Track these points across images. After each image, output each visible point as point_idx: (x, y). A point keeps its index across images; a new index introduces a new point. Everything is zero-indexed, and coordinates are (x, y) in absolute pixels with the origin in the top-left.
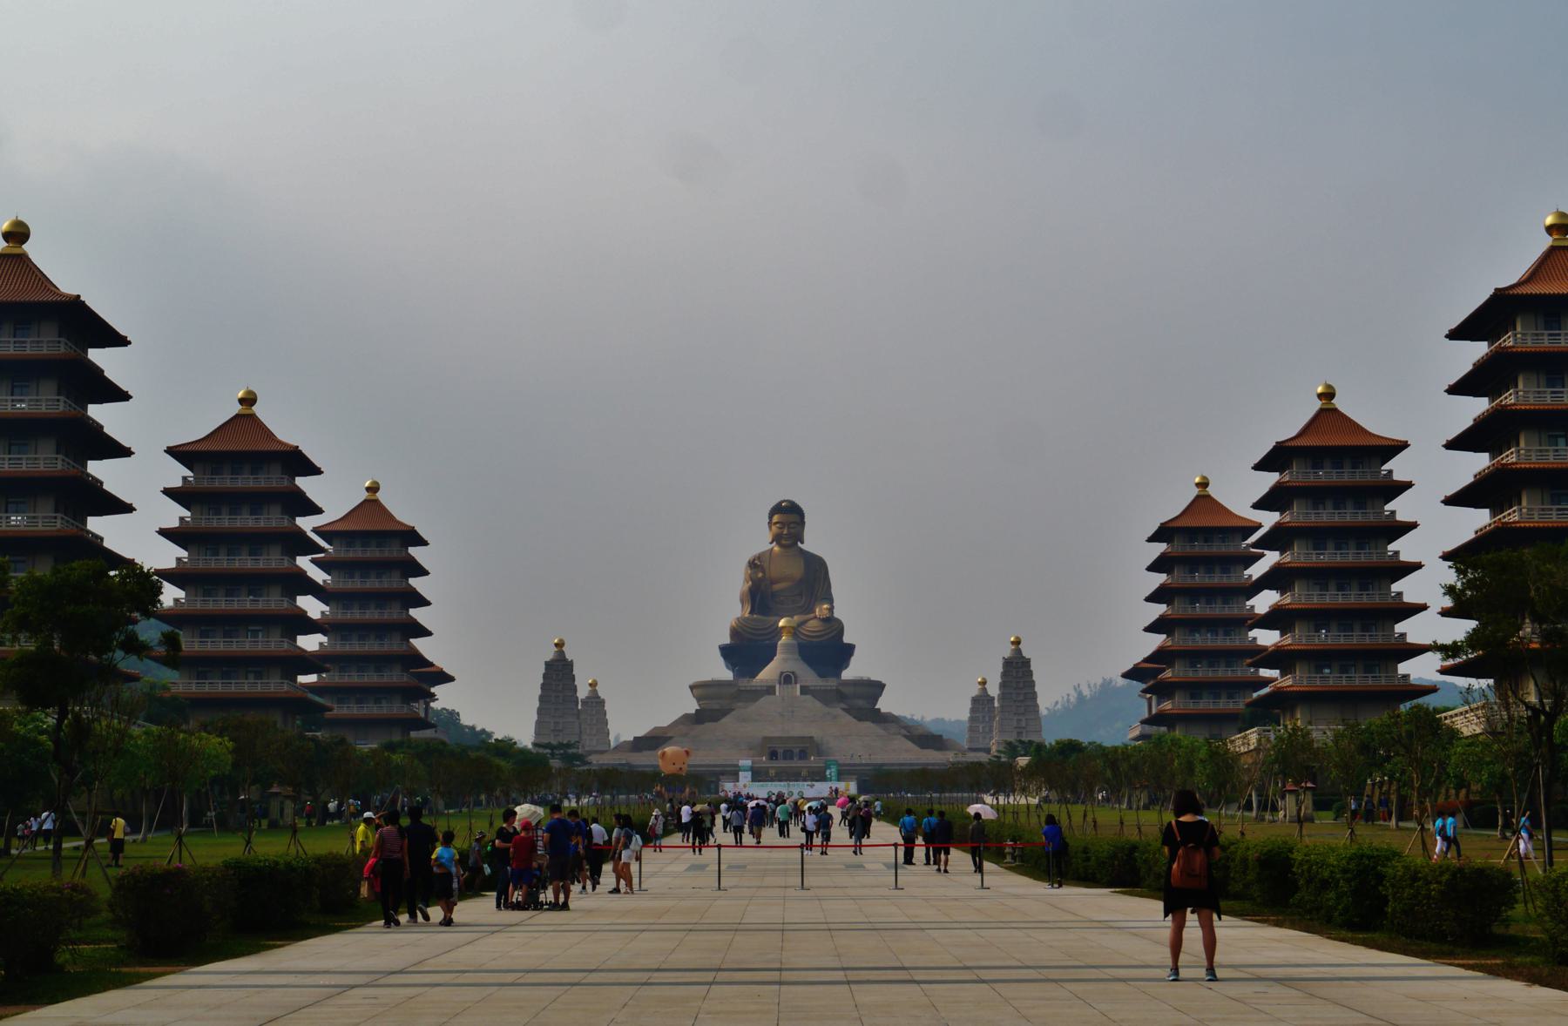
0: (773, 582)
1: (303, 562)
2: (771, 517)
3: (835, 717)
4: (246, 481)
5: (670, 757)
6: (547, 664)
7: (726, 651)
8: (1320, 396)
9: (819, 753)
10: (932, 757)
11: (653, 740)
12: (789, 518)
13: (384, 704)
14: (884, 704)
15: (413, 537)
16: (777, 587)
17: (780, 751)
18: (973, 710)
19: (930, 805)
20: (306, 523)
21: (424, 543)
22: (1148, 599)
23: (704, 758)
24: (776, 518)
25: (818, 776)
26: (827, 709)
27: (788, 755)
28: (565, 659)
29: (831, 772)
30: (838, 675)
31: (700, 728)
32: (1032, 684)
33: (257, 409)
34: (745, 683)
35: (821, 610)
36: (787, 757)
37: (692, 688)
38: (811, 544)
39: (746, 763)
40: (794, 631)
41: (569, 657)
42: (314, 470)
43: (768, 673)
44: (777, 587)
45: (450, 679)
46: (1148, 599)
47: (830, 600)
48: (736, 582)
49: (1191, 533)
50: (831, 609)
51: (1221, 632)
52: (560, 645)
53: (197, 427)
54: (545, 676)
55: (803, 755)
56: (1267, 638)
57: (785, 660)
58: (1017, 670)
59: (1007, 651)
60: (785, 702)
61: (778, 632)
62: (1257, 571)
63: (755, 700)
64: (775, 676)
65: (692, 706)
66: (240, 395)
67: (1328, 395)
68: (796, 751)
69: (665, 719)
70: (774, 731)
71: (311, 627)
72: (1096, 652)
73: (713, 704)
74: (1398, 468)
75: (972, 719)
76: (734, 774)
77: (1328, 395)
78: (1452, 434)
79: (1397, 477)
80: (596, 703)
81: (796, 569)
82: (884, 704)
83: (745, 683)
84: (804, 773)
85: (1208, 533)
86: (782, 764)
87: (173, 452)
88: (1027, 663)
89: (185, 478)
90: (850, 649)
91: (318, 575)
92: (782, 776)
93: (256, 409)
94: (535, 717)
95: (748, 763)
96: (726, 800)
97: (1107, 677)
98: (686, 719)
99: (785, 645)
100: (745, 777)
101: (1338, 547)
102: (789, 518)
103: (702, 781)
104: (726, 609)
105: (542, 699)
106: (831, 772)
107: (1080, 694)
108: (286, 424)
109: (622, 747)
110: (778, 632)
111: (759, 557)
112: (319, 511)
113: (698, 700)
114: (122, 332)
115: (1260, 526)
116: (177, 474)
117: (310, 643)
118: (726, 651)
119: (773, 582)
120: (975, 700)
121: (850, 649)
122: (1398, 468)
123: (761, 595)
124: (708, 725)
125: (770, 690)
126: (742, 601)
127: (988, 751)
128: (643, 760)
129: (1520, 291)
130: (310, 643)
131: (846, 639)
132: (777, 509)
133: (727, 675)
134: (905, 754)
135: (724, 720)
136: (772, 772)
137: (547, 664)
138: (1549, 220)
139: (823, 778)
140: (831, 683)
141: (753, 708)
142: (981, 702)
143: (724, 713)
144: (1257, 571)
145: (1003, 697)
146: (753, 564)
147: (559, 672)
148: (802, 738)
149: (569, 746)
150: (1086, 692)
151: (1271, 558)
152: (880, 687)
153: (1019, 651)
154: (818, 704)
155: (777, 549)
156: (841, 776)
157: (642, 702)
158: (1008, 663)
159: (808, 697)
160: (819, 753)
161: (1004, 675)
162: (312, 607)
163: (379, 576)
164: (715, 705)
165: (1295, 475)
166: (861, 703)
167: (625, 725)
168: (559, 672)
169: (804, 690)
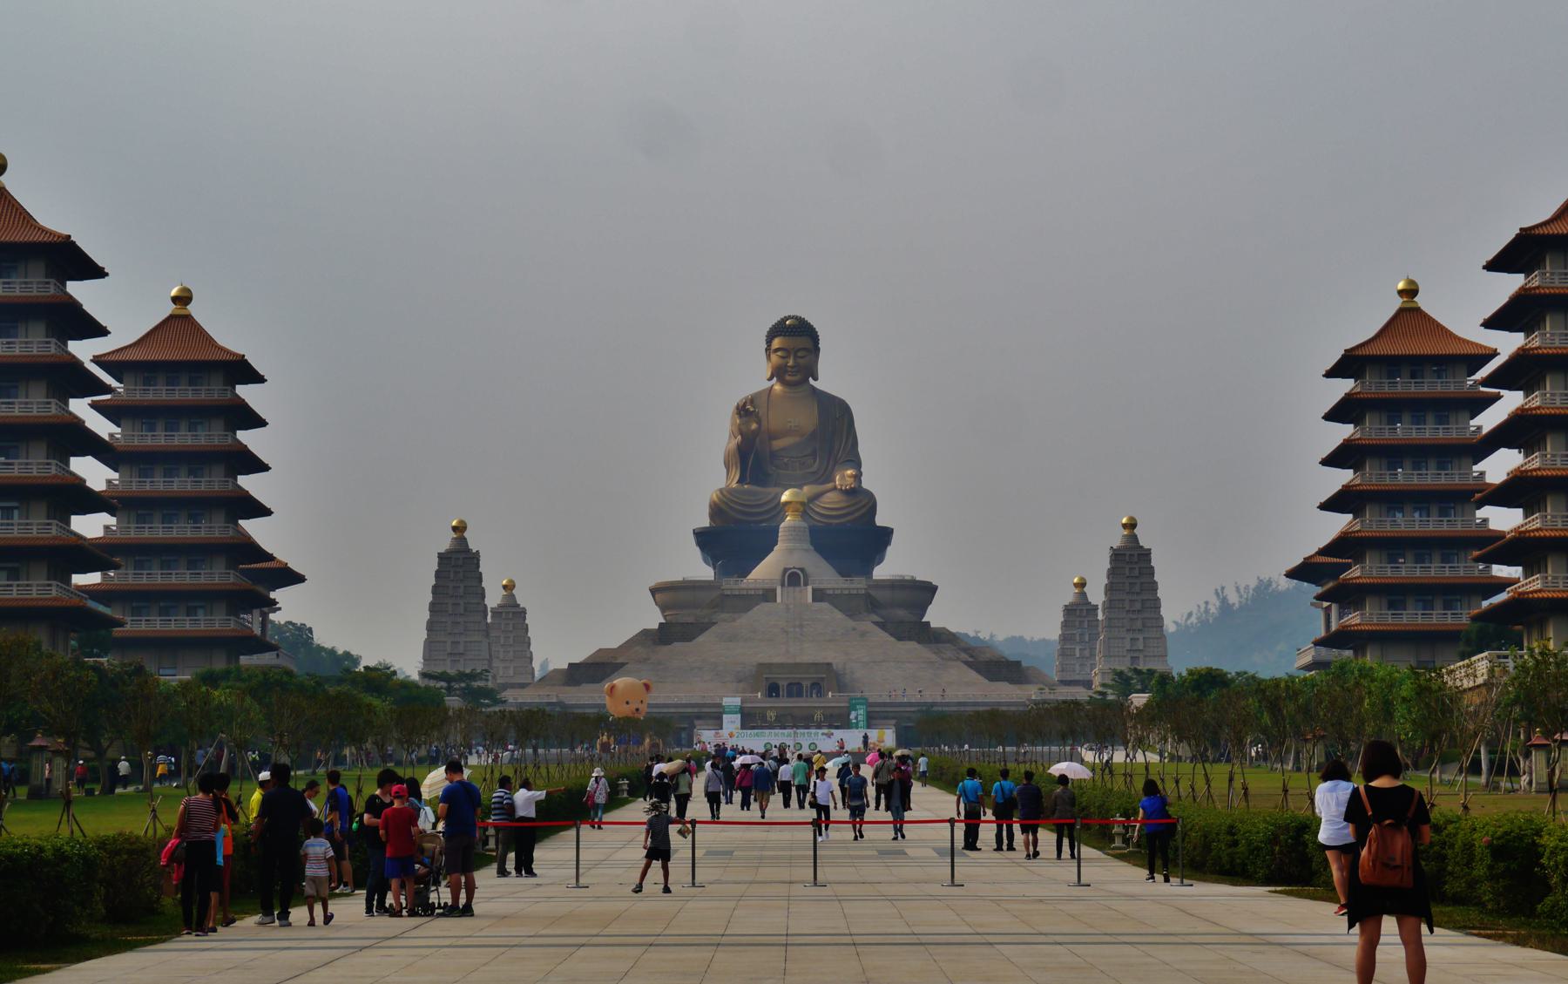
0: (773, 436)
1: (80, 407)
3: (863, 634)
5: (621, 694)
6: (441, 556)
7: (704, 539)
8: (1401, 293)
9: (841, 687)
10: (1005, 694)
11: (596, 669)
12: (796, 342)
13: (201, 615)
14: (935, 616)
15: (71, 260)
17: (783, 684)
18: (1065, 625)
20: (83, 350)
23: (672, 694)
24: (776, 343)
26: (851, 623)
27: (795, 690)
28: (469, 551)
29: (858, 714)
30: (869, 573)
32: (1153, 587)
33: (192, 309)
34: (731, 585)
35: (844, 477)
36: (791, 693)
37: (653, 591)
38: (828, 380)
40: (804, 509)
41: (473, 546)
42: (256, 378)
43: (766, 570)
47: (857, 464)
48: (721, 436)
50: (858, 477)
52: (460, 529)
54: (438, 574)
55: (817, 688)
56: (1504, 519)
57: (790, 551)
58: (1132, 566)
59: (1117, 538)
61: (779, 510)
62: (1489, 420)
63: (747, 609)
65: (653, 618)
66: (174, 292)
71: (90, 502)
72: (1248, 537)
73: (684, 615)
75: (1065, 638)
76: (715, 717)
77: (1410, 292)
80: (513, 613)
81: (805, 418)
82: (935, 616)
83: (731, 585)
84: (818, 716)
85: (1417, 364)
86: (785, 703)
88: (1146, 555)
90: (885, 535)
91: (102, 427)
92: (782, 721)
95: (737, 701)
98: (647, 638)
99: (793, 529)
100: (731, 722)
102: (796, 342)
104: (709, 476)
105: (433, 607)
106: (858, 714)
107: (1224, 601)
108: (227, 329)
109: (551, 678)
110: (779, 510)
111: (752, 400)
112: (101, 331)
115: (1494, 354)
117: (90, 526)
118: (704, 539)
119: (773, 436)
120: (1069, 610)
121: (885, 535)
123: (754, 455)
125: (768, 595)
128: (583, 697)
129: (1545, 231)
130: (90, 526)
131: (880, 521)
132: (778, 330)
134: (966, 689)
135: (701, 639)
136: (771, 715)
137: (441, 556)
138: (1401, 285)
139: (845, 724)
140: (858, 584)
141: (744, 620)
142: (1078, 612)
144: (1489, 420)
145: (1110, 605)
146: (743, 411)
147: (458, 568)
148: (815, 666)
149: (473, 676)
150: (1233, 598)
151: (1511, 401)
152: (928, 590)
153: (1134, 538)
154: (839, 615)
155: (778, 387)
156: (872, 720)
158: (1117, 556)
159: (825, 605)
160: (841, 687)
161: (1112, 573)
162: (93, 473)
164: (686, 617)
165: (1377, 385)
166: (901, 613)
167: (554, 647)
168: (458, 568)
169: (819, 595)
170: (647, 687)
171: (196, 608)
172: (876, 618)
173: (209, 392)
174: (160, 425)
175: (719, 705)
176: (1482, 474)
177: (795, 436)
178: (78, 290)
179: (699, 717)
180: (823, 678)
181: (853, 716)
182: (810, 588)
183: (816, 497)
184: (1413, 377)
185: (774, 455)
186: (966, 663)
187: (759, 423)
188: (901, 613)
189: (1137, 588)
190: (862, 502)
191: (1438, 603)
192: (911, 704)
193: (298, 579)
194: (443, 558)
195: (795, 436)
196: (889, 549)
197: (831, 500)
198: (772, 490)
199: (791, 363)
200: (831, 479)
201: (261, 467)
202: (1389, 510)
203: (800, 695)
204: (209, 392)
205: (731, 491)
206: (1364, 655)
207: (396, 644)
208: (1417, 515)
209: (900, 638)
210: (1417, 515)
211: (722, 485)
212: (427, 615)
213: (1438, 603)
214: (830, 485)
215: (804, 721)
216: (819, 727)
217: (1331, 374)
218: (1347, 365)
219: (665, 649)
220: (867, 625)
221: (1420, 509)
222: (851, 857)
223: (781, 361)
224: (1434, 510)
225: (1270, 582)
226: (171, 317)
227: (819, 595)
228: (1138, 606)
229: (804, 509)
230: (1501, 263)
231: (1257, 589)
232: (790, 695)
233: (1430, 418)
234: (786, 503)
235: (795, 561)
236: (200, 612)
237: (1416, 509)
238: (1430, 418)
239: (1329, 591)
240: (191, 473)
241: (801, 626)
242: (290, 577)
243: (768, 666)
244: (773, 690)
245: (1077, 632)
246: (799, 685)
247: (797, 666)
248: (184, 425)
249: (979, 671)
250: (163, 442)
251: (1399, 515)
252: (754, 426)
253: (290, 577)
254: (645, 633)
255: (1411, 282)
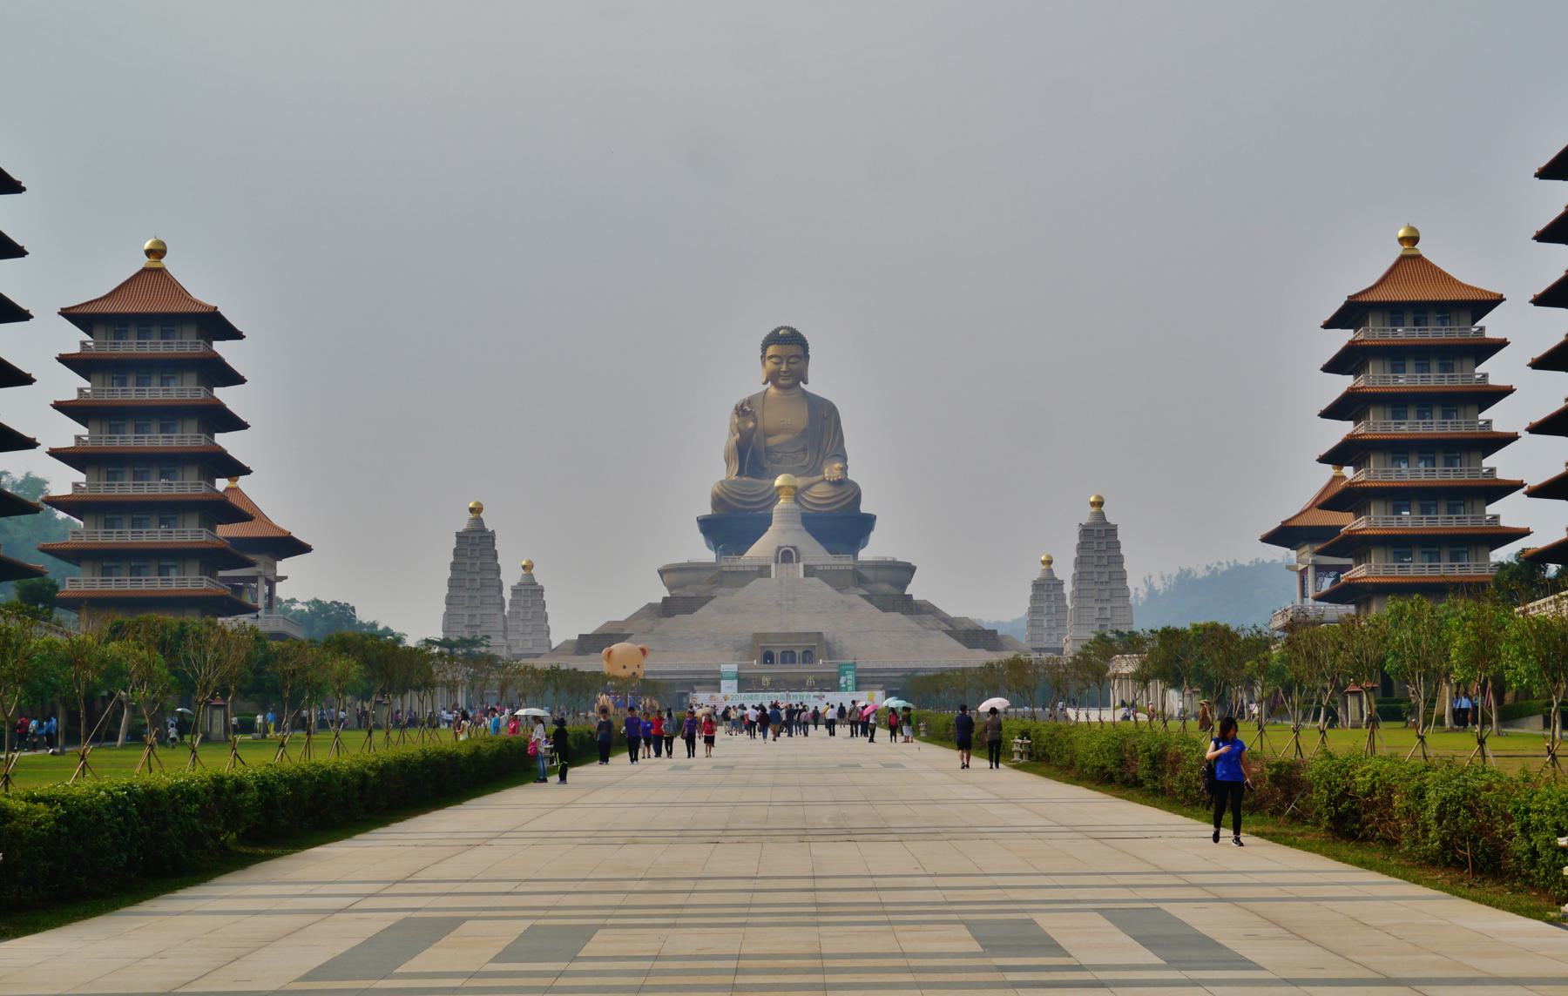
2: (764, 350)
3: (851, 606)
4: (155, 347)
5: (620, 659)
6: (460, 536)
7: (708, 526)
8: (1402, 240)
9: (831, 654)
12: (788, 350)
13: (173, 575)
14: (917, 590)
15: (216, 325)
16: (772, 441)
17: (777, 652)
18: (1034, 598)
19: (973, 711)
21: (236, 335)
22: (1326, 414)
23: (665, 662)
24: (771, 350)
25: (829, 683)
26: (840, 596)
27: (789, 657)
28: (483, 530)
29: (848, 679)
30: (855, 555)
31: (667, 622)
32: (1119, 560)
34: (732, 562)
35: (831, 471)
36: (784, 657)
37: (662, 572)
38: (818, 382)
39: (730, 667)
40: (797, 494)
41: (489, 526)
43: (761, 549)
44: (772, 441)
45: (302, 548)
46: (1326, 414)
48: (720, 435)
49: (1396, 311)
50: (844, 469)
51: (1440, 459)
52: (476, 510)
53: (97, 282)
54: (456, 552)
55: (808, 656)
58: (1099, 541)
59: (1086, 516)
60: (785, 591)
63: (744, 585)
64: (771, 553)
65: (658, 592)
66: (147, 245)
67: (1412, 240)
68: (799, 652)
69: (621, 610)
70: (771, 624)
72: (1225, 502)
73: (685, 594)
74: (1492, 325)
75: (1034, 611)
76: (714, 684)
77: (1412, 240)
78: (1540, 289)
79: (1489, 334)
80: (530, 591)
81: (797, 418)
82: (917, 590)
83: (732, 562)
84: (810, 681)
85: (1419, 311)
86: (778, 669)
87: (67, 314)
88: (1112, 531)
89: (83, 343)
90: (868, 522)
92: (775, 686)
93: (166, 262)
94: (444, 608)
96: (1132, 643)
97: (1185, 567)
99: (786, 511)
100: (729, 688)
101: (1421, 416)
102: (788, 350)
103: (677, 689)
104: (709, 470)
105: (452, 583)
106: (848, 679)
107: (1151, 587)
108: (202, 284)
111: (749, 401)
113: (670, 589)
114: (16, 177)
116: (74, 339)
118: (708, 526)
119: (767, 435)
120: (1037, 586)
121: (868, 522)
122: (1492, 325)
123: (751, 453)
124: (680, 618)
125: (763, 571)
126: (727, 460)
127: (1060, 651)
131: (865, 508)
132: (774, 339)
133: (707, 555)
135: (700, 612)
136: (766, 680)
137: (460, 536)
138: (1401, 233)
139: (836, 688)
140: (844, 561)
142: (1046, 587)
143: (702, 601)
145: (1079, 578)
146: (742, 411)
147: (475, 547)
149: (473, 642)
150: (1159, 586)
152: (909, 570)
154: (828, 589)
155: (773, 390)
156: (859, 684)
157: (589, 591)
158: (1086, 532)
159: (815, 580)
161: (1082, 547)
163: (164, 382)
164: (689, 592)
165: (1373, 333)
166: (885, 588)
168: (475, 547)
169: (810, 571)
170: (643, 651)
171: (168, 567)
172: (862, 591)
173: (185, 345)
174: (131, 379)
175: (718, 672)
176: (1489, 422)
177: (787, 438)
178: (221, 348)
179: (699, 683)
180: (811, 648)
181: (842, 680)
182: (801, 565)
183: (809, 487)
184: (1416, 324)
185: (768, 451)
186: (946, 632)
187: (755, 421)
188: (885, 588)
189: (1105, 561)
190: (849, 493)
191: (1445, 554)
192: (895, 670)
193: (302, 548)
194: (461, 537)
195: (787, 438)
196: (872, 534)
197: (820, 491)
198: (767, 482)
199: (784, 368)
200: (819, 471)
201: (239, 425)
202: (1394, 460)
203: (793, 661)
204: (185, 345)
205: (731, 483)
206: (1368, 609)
207: (415, 615)
208: (1422, 465)
209: (885, 610)
210: (1422, 465)
211: (723, 477)
212: (445, 590)
213: (1445, 554)
214: (820, 477)
215: (799, 685)
216: (811, 690)
217: (1330, 324)
218: (1350, 314)
219: (667, 621)
220: (855, 597)
221: (1426, 459)
222: (890, 923)
223: (774, 367)
224: (1440, 459)
225: (1189, 572)
226: (144, 270)
227: (810, 571)
228: (1105, 578)
229: (797, 494)
230: (1337, 321)
231: (1179, 577)
232: (784, 661)
233: (1434, 365)
234: (780, 487)
235: (788, 540)
236: (173, 571)
237: (1421, 459)
238: (1434, 365)
239: (1331, 546)
240: (164, 429)
241: (794, 599)
242: (292, 546)
243: (764, 636)
244: (768, 657)
245: (1045, 605)
246: (792, 652)
247: (788, 636)
248: (156, 379)
249: (958, 639)
250: (133, 397)
251: (1404, 466)
252: (751, 424)
253: (292, 546)
254: (650, 607)
255: (1413, 229)
